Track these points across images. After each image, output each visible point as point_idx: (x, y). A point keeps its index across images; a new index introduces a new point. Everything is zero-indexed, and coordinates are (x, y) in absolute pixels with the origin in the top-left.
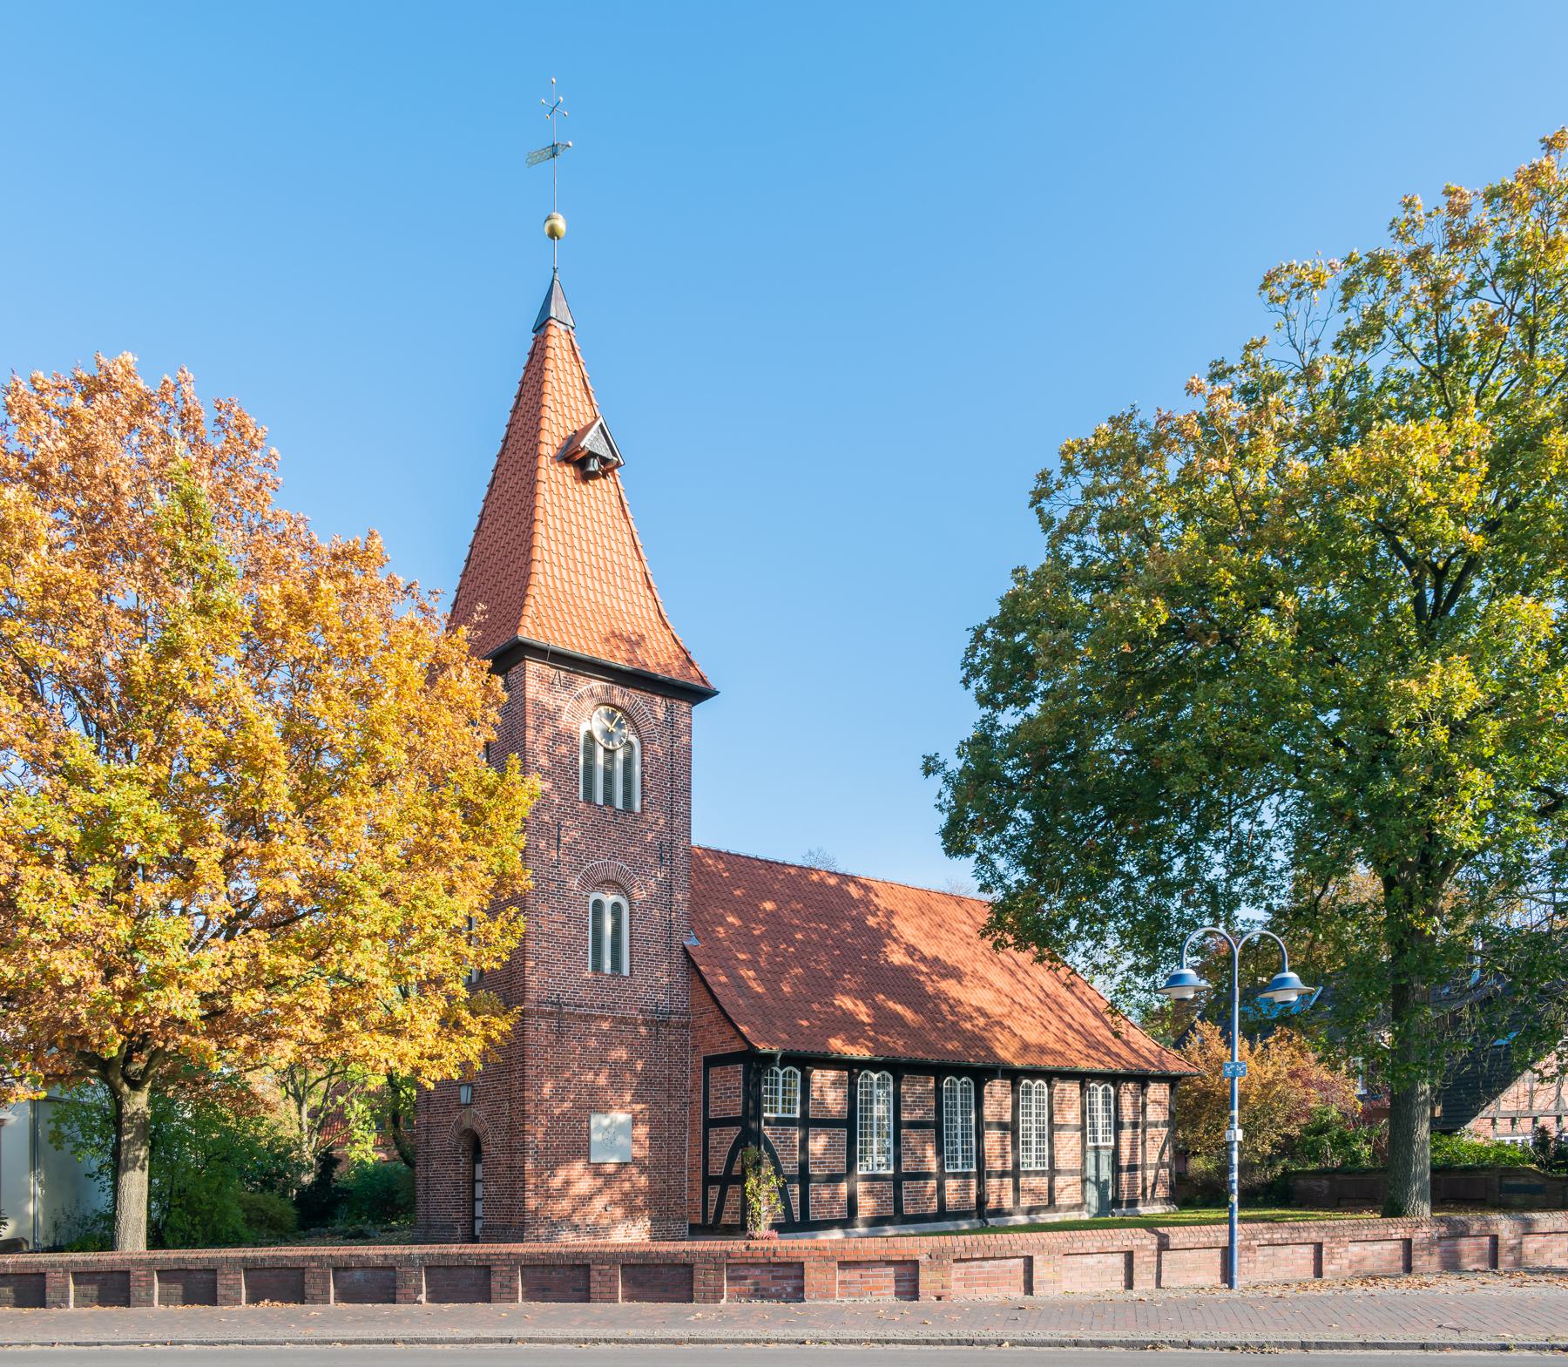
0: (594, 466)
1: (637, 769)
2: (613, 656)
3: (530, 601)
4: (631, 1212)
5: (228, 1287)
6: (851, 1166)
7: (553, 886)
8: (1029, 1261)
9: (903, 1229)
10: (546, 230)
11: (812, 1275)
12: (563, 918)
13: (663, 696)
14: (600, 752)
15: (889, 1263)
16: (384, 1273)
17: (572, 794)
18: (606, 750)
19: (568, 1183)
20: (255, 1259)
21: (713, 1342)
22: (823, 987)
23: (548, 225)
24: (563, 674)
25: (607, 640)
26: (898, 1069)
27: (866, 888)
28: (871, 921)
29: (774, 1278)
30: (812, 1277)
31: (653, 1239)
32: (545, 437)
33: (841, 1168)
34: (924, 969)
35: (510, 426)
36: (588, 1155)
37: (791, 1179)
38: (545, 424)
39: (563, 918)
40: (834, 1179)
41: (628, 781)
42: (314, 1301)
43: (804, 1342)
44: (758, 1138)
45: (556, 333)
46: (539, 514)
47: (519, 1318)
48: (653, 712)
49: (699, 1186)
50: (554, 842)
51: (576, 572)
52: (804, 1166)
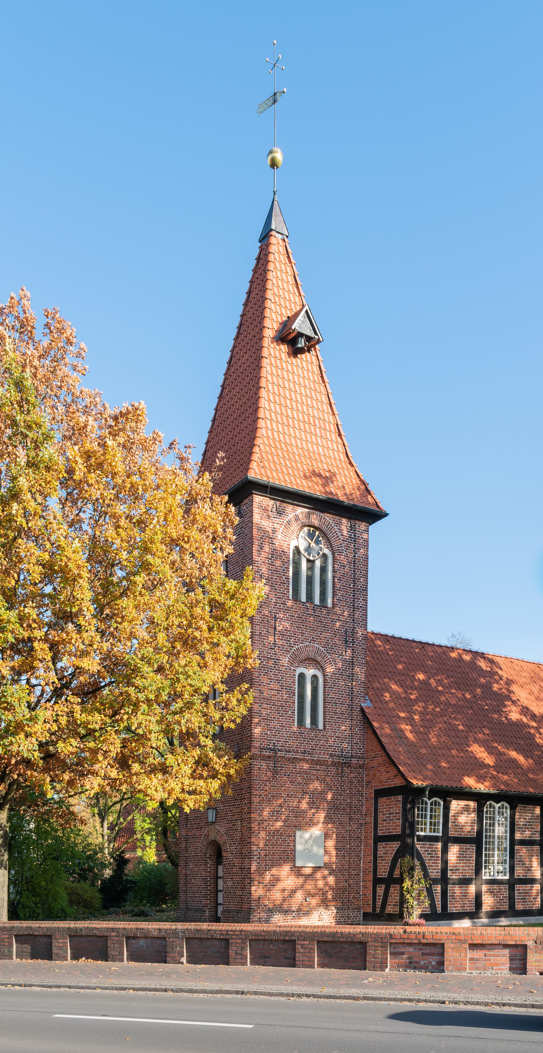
0: (301, 343)
1: (330, 575)
3: (256, 449)
4: (324, 903)
6: (478, 871)
7: (271, 662)
11: (450, 953)
13: (349, 518)
15: (506, 946)
18: (308, 561)
19: (277, 879)
20: (76, 929)
27: (491, 661)
30: (450, 954)
31: (338, 923)
32: (267, 323)
33: (470, 873)
34: (534, 724)
35: (242, 316)
36: (294, 861)
37: (435, 881)
38: (267, 313)
39: (277, 687)
41: (323, 583)
46: (263, 383)
52: (444, 871)
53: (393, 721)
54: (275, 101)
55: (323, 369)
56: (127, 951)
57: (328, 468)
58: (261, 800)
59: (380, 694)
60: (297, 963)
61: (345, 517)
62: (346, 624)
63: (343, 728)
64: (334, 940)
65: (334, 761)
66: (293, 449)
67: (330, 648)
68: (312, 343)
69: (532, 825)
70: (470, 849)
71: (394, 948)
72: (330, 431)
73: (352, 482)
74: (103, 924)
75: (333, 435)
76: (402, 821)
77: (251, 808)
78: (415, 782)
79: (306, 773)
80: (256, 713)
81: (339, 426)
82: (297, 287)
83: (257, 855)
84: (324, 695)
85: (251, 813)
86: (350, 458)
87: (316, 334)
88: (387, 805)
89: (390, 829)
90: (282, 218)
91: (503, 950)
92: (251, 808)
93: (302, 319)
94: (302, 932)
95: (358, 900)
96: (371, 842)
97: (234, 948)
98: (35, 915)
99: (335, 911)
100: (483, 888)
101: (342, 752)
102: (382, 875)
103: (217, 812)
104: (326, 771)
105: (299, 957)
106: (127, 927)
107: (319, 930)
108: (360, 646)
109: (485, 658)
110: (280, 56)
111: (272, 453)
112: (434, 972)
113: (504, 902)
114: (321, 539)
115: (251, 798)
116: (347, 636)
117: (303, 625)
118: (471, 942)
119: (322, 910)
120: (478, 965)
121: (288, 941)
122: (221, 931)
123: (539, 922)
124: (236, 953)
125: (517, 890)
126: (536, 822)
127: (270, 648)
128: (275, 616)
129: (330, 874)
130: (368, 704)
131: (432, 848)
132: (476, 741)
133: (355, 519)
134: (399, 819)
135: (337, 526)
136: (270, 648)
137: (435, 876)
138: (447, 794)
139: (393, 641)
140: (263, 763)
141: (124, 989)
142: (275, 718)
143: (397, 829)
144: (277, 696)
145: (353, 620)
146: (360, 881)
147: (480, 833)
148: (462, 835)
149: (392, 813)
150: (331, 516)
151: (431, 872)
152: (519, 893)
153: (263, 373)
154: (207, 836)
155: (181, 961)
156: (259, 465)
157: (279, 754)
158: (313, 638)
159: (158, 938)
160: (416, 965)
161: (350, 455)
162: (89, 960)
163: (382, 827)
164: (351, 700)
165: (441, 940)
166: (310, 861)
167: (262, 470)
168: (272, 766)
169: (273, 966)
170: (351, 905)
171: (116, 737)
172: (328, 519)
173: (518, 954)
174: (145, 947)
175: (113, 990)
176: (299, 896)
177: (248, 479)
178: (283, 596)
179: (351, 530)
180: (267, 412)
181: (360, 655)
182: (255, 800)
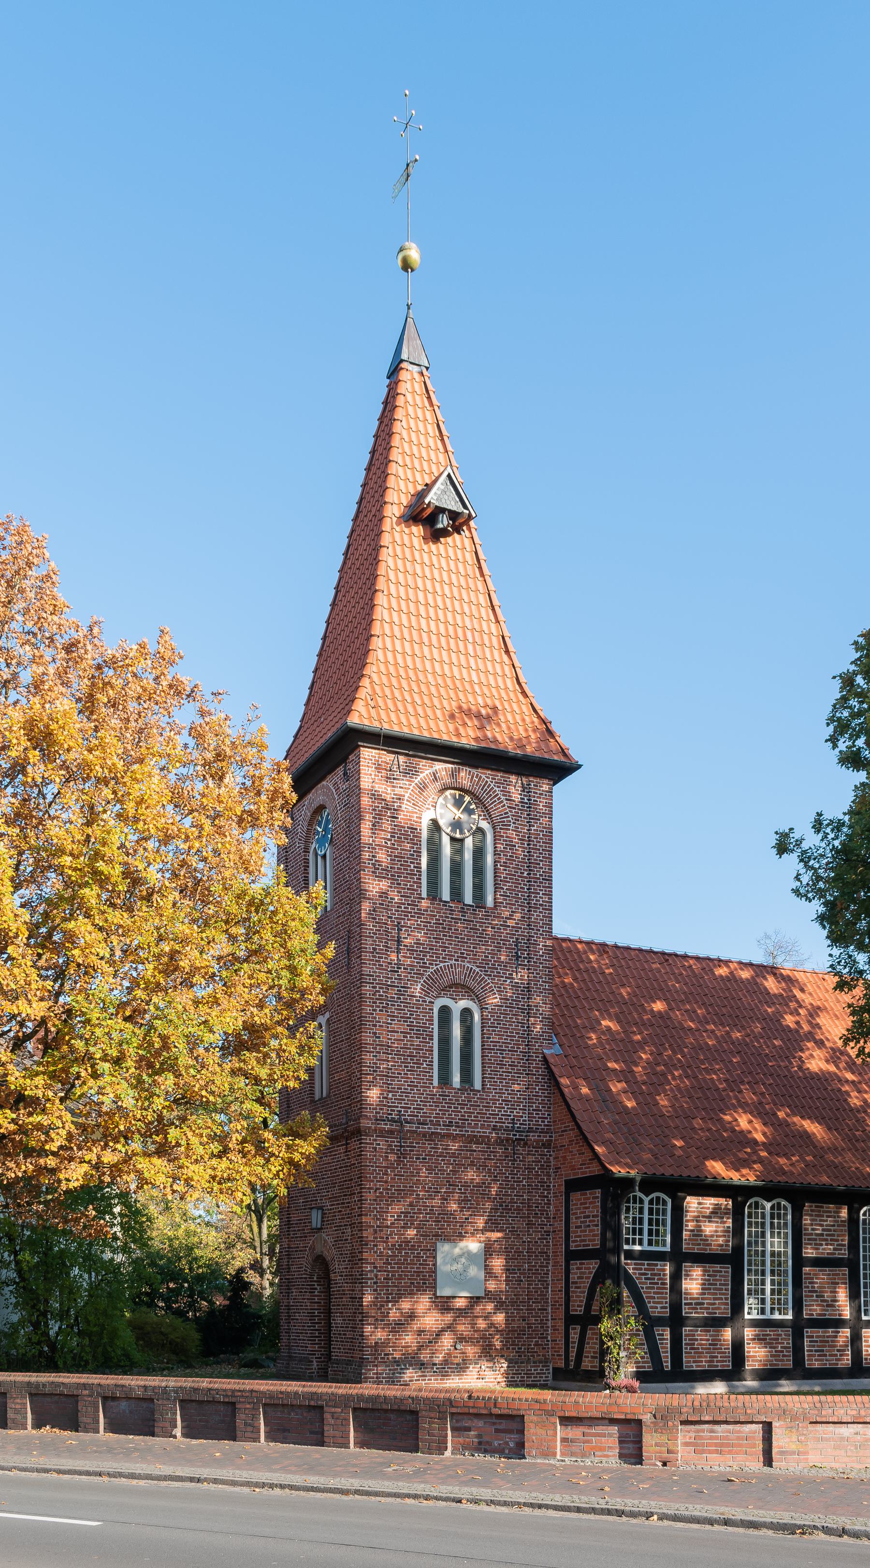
0: (443, 522)
1: (489, 859)
2: (458, 735)
3: (365, 682)
4: (488, 1353)
5: (16, 1411)
6: (737, 1306)
7: (393, 992)
8: (768, 1428)
9: (806, 1385)
10: (400, 263)
11: (532, 1430)
12: (404, 1027)
13: (519, 774)
14: (446, 840)
15: (613, 1421)
16: (145, 1405)
17: (415, 890)
18: (453, 839)
19: (412, 1316)
20: (37, 1385)
21: (377, 1494)
22: (713, 1102)
23: (400, 256)
24: (402, 759)
25: (452, 716)
26: (799, 1196)
27: (789, 980)
28: (789, 1020)
29: (497, 1431)
30: (533, 1432)
31: (511, 1383)
32: (391, 496)
33: (723, 1309)
34: (850, 1076)
35: (364, 486)
36: (434, 1287)
37: (660, 1321)
38: (391, 482)
39: (404, 1027)
40: (715, 1323)
42: (86, 1431)
43: (460, 1501)
44: (616, 1274)
45: (409, 377)
46: (381, 584)
47: (352, 1466)
48: (506, 793)
49: (561, 1325)
50: (393, 945)
51: (422, 643)
52: (676, 1307)
53: (598, 1077)
54: (408, 176)
55: (482, 556)
56: (105, 1417)
57: (485, 702)
58: (378, 1197)
59: (578, 1035)
60: (326, 1439)
61: (512, 773)
62: (517, 931)
63: (516, 1087)
64: (374, 1407)
65: (500, 1138)
66: (426, 677)
67: (489, 967)
68: (461, 520)
69: (834, 1235)
70: (721, 1272)
71: (457, 1421)
72: (491, 647)
73: (523, 720)
74: (73, 1377)
75: (496, 653)
76: (602, 1228)
77: (361, 1208)
78: (615, 1169)
79: (453, 1155)
80: (369, 1067)
81: (507, 639)
82: (442, 440)
83: (372, 1279)
84: (483, 1038)
85: (361, 1215)
86: (523, 684)
87: (465, 507)
88: (581, 1204)
89: (585, 1241)
90: (419, 342)
91: (610, 1428)
92: (361, 1208)
93: (442, 487)
94: (332, 1394)
95: (544, 1348)
96: (562, 1260)
97: (243, 1416)
98: (83, 1363)
99: (505, 1365)
100: (746, 1333)
101: (513, 1123)
102: (576, 1311)
103: (323, 1214)
104: (487, 1152)
105: (329, 1431)
106: (103, 1382)
107: (442, 1395)
108: (541, 963)
109: (775, 974)
110: (413, 112)
111: (391, 686)
112: (511, 1458)
113: (784, 1356)
114: (473, 806)
115: (361, 1192)
116: (519, 950)
117: (444, 935)
118: (562, 1414)
119: (485, 1365)
120: (574, 1449)
121: (314, 1407)
122: (225, 1390)
123: (848, 1388)
124: (246, 1424)
125: (808, 1337)
126: (842, 1230)
127: (391, 971)
128: (399, 923)
129: (497, 1309)
130: (557, 1049)
131: (653, 1270)
132: (745, 1107)
133: (527, 776)
134: (597, 1225)
135: (499, 787)
136: (391, 971)
137: (659, 1312)
138: (680, 1187)
139: (615, 953)
140: (382, 1141)
141: (46, 1471)
142: (400, 1074)
143: (594, 1240)
144: (403, 1040)
145: (528, 925)
146: (547, 1320)
147: (738, 1250)
148: (706, 1250)
149: (588, 1217)
150: (490, 772)
151: (652, 1307)
152: (810, 1342)
153: (382, 570)
154: (313, 1248)
155: (173, 1433)
156: (367, 704)
157: (407, 1127)
158: (462, 953)
159: (143, 1399)
160: (487, 1447)
161: (522, 679)
162: (54, 1430)
163: (576, 1237)
164: (527, 1045)
165: (519, 1410)
166: (463, 1290)
167: (373, 712)
168: (396, 1146)
169: (312, 1445)
170: (533, 1356)
171: (62, 1107)
172: (483, 776)
173: (631, 1433)
174: (127, 1411)
175: (33, 1472)
176: (447, 1341)
177: (347, 727)
178: (411, 893)
179: (523, 791)
180: (386, 626)
181: (541, 977)
182: (369, 1196)
